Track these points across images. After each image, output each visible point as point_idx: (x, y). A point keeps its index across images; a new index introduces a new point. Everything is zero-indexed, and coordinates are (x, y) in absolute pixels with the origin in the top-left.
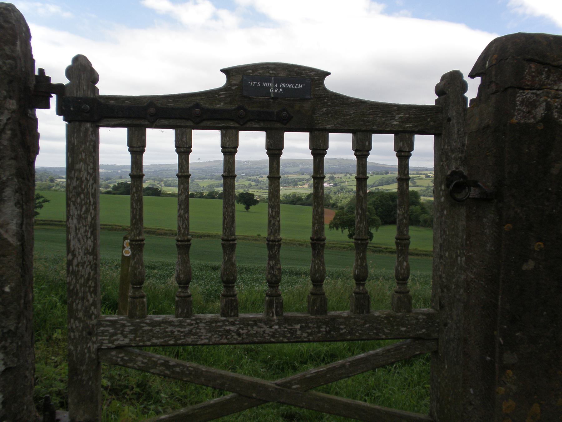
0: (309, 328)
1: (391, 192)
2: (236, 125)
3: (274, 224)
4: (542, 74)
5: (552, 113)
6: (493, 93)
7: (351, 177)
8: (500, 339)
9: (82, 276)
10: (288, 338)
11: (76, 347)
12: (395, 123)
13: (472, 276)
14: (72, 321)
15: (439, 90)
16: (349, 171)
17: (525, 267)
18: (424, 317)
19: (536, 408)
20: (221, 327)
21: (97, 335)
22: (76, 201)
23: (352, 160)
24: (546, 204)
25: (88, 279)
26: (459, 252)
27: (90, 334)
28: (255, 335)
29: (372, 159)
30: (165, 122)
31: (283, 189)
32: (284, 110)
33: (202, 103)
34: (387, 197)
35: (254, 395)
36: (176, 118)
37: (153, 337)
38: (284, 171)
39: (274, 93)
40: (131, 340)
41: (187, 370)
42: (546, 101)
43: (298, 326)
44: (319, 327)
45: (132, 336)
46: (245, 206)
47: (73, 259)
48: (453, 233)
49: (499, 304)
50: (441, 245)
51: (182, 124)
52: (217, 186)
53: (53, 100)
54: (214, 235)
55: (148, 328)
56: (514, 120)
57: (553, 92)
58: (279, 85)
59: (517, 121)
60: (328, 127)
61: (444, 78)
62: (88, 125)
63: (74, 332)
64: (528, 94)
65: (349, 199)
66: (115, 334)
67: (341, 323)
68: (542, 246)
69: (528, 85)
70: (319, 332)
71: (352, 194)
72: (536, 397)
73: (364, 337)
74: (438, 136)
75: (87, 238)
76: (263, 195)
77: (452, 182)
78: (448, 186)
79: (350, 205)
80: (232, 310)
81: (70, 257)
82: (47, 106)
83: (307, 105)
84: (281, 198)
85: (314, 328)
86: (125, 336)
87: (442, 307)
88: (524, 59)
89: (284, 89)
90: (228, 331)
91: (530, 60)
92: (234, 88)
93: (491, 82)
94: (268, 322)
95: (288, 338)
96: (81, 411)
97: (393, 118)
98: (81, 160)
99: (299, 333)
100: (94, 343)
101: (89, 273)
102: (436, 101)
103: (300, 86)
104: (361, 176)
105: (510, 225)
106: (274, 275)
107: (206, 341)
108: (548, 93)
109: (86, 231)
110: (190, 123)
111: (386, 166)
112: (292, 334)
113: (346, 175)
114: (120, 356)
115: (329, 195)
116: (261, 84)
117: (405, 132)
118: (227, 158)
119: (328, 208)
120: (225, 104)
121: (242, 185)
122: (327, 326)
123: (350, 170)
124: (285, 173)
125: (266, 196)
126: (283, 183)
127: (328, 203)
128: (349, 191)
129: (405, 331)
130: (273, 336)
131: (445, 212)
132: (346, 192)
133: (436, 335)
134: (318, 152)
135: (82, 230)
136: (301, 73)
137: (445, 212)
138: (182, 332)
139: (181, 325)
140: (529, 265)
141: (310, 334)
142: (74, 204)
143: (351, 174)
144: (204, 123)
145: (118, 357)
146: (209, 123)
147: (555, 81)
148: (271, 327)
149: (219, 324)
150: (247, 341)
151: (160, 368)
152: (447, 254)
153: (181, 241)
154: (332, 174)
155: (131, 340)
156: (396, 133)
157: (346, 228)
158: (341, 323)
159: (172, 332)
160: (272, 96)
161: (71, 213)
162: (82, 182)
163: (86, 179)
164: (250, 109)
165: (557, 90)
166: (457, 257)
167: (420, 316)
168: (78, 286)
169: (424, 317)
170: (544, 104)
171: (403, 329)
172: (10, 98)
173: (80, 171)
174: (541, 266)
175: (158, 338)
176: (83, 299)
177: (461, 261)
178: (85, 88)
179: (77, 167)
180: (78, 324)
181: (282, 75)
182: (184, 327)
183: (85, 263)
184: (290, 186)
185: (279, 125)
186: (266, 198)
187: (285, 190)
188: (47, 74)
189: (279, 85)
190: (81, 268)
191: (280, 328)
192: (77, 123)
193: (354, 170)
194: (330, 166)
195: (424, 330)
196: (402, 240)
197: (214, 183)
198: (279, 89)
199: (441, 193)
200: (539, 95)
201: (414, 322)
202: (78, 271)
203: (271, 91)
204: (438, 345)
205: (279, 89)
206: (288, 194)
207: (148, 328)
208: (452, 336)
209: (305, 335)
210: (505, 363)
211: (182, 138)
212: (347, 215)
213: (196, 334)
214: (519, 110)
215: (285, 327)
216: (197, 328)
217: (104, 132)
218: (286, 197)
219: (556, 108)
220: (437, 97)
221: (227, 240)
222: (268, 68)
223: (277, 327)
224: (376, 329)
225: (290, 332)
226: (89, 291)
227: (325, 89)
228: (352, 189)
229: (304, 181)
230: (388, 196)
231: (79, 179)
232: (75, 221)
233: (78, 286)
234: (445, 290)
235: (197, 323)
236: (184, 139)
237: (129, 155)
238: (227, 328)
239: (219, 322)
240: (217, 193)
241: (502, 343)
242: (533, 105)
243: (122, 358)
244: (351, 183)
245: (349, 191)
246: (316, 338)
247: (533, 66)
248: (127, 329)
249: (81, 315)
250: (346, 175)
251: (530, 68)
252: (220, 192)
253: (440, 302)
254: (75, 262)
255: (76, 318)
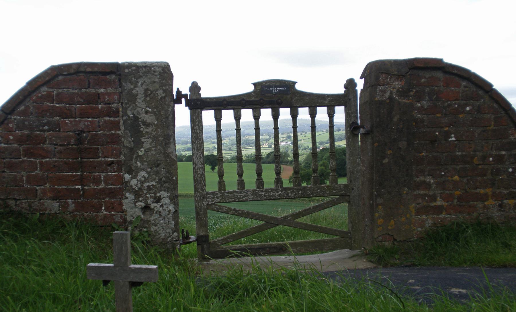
0: (294, 192)
1: (343, 147)
2: (260, 107)
3: (277, 148)
4: (388, 78)
5: (393, 95)
6: (369, 87)
7: (306, 135)
8: (375, 193)
9: (199, 173)
10: (286, 197)
11: (198, 204)
12: (327, 102)
13: (365, 169)
14: (196, 192)
15: (345, 86)
16: (304, 130)
17: (384, 162)
18: (344, 186)
19: (392, 222)
20: (257, 193)
21: (207, 198)
22: (196, 142)
23: (306, 120)
24: (392, 134)
25: (202, 175)
26: (357, 157)
27: (204, 198)
28: (271, 196)
29: (261, 119)
30: (231, 107)
31: (244, 150)
32: (279, 99)
33: (245, 98)
34: (341, 152)
35: (272, 222)
36: (235, 105)
37: (229, 198)
38: (244, 133)
39: (275, 92)
40: (220, 200)
41: (244, 212)
42: (390, 90)
43: (290, 192)
44: (298, 192)
45: (221, 198)
46: (211, 167)
47: (195, 166)
48: (354, 149)
49: (374, 177)
50: (349, 155)
51: (237, 108)
52: (183, 150)
53: (183, 100)
54: (185, 195)
55: (227, 194)
56: (377, 99)
57: (393, 86)
58: (276, 89)
59: (377, 99)
60: (298, 105)
61: (347, 81)
62: (199, 110)
63: (197, 197)
64: (382, 87)
65: (305, 156)
66: (214, 198)
67: (308, 190)
68: (391, 152)
69: (382, 84)
70: (299, 194)
71: (308, 151)
72: (392, 217)
73: (318, 196)
74: (346, 107)
75: (201, 158)
76: (226, 156)
77: (352, 126)
78: (350, 128)
79: (306, 161)
80: (261, 186)
81: (194, 166)
82: (181, 103)
83: (289, 97)
84: (244, 158)
85: (296, 192)
86: (218, 198)
87: (351, 181)
88: (380, 73)
89: (279, 90)
90: (260, 195)
91: (382, 73)
92: (258, 91)
93: (368, 82)
94: (277, 190)
95: (286, 197)
96: (202, 231)
97: (325, 100)
98: (197, 125)
99: (290, 194)
100: (205, 202)
101: (202, 172)
102: (345, 91)
103: (286, 89)
104: (313, 126)
105: (377, 144)
106: (278, 170)
107: (251, 199)
108: (391, 86)
109: (200, 155)
110: (240, 107)
111: (338, 124)
112: (287, 195)
113: (302, 134)
114: (216, 207)
115: (287, 153)
116: (269, 89)
117: (331, 106)
118: (256, 121)
119: (286, 165)
120: (255, 98)
121: (207, 148)
122: (302, 191)
123: (306, 129)
124: (246, 135)
125: (229, 157)
126: (244, 144)
127: (287, 160)
128: (305, 149)
129: (336, 192)
130: (279, 196)
131: (350, 140)
132: (303, 149)
133: (348, 194)
134: (294, 116)
135: (199, 154)
136: (286, 83)
137: (350, 140)
138: (241, 196)
139: (241, 193)
140: (386, 161)
141: (295, 195)
142: (195, 144)
143: (306, 133)
144: (246, 107)
145: (215, 208)
146: (248, 106)
147: (394, 81)
148: (278, 192)
149: (256, 192)
150: (268, 199)
151: (233, 212)
152: (352, 158)
153: (239, 157)
154: (288, 133)
155: (220, 200)
156: (328, 106)
157: (305, 182)
158: (308, 190)
159: (237, 196)
160: (274, 93)
161: (194, 147)
162: (197, 134)
163: (199, 133)
164: (265, 99)
165: (395, 85)
166: (356, 159)
167: (342, 186)
168: (198, 178)
169: (344, 186)
170: (389, 91)
171: (335, 191)
172: (172, 102)
173: (197, 129)
174: (391, 161)
175: (231, 199)
176: (200, 183)
177: (358, 161)
178: (197, 95)
179: (195, 128)
180: (199, 194)
181: (278, 84)
182: (242, 193)
183: (200, 168)
184: (251, 146)
185: (277, 106)
186: (229, 159)
187: (247, 150)
188: (180, 90)
189: (276, 89)
190: (199, 170)
191: (282, 192)
192: (195, 110)
193: (309, 129)
194: (286, 126)
195: (344, 192)
196: (332, 153)
197: (181, 147)
198: (277, 90)
199: (348, 132)
200: (387, 87)
201: (339, 188)
202: (198, 172)
203: (273, 91)
204: (350, 198)
205: (277, 90)
206: (250, 154)
207: (227, 194)
208: (356, 194)
209: (293, 195)
210: (378, 203)
211: (237, 113)
212: (305, 171)
213: (247, 196)
214: (378, 94)
215: (284, 192)
216: (248, 194)
217: (204, 112)
218: (248, 157)
219: (395, 92)
220: (345, 89)
221: (258, 156)
222: (272, 82)
223: (281, 192)
224: (323, 192)
225: (286, 194)
226: (203, 180)
227: (296, 89)
228: (308, 147)
229: (263, 141)
230: (341, 151)
231: (196, 133)
232: (196, 151)
233: (198, 178)
234: (352, 174)
235: (247, 192)
236: (238, 114)
237: (328, 118)
238: (260, 193)
239: (256, 191)
240: (184, 156)
241: (376, 194)
242: (384, 92)
243: (217, 208)
244: (307, 141)
245: (305, 149)
246: (297, 197)
247: (384, 75)
248: (219, 195)
249: (199, 190)
250: (302, 134)
251: (383, 76)
252: (186, 155)
253: (350, 179)
254: (196, 168)
255: (198, 191)
